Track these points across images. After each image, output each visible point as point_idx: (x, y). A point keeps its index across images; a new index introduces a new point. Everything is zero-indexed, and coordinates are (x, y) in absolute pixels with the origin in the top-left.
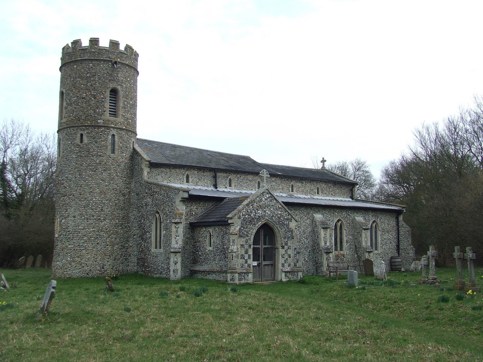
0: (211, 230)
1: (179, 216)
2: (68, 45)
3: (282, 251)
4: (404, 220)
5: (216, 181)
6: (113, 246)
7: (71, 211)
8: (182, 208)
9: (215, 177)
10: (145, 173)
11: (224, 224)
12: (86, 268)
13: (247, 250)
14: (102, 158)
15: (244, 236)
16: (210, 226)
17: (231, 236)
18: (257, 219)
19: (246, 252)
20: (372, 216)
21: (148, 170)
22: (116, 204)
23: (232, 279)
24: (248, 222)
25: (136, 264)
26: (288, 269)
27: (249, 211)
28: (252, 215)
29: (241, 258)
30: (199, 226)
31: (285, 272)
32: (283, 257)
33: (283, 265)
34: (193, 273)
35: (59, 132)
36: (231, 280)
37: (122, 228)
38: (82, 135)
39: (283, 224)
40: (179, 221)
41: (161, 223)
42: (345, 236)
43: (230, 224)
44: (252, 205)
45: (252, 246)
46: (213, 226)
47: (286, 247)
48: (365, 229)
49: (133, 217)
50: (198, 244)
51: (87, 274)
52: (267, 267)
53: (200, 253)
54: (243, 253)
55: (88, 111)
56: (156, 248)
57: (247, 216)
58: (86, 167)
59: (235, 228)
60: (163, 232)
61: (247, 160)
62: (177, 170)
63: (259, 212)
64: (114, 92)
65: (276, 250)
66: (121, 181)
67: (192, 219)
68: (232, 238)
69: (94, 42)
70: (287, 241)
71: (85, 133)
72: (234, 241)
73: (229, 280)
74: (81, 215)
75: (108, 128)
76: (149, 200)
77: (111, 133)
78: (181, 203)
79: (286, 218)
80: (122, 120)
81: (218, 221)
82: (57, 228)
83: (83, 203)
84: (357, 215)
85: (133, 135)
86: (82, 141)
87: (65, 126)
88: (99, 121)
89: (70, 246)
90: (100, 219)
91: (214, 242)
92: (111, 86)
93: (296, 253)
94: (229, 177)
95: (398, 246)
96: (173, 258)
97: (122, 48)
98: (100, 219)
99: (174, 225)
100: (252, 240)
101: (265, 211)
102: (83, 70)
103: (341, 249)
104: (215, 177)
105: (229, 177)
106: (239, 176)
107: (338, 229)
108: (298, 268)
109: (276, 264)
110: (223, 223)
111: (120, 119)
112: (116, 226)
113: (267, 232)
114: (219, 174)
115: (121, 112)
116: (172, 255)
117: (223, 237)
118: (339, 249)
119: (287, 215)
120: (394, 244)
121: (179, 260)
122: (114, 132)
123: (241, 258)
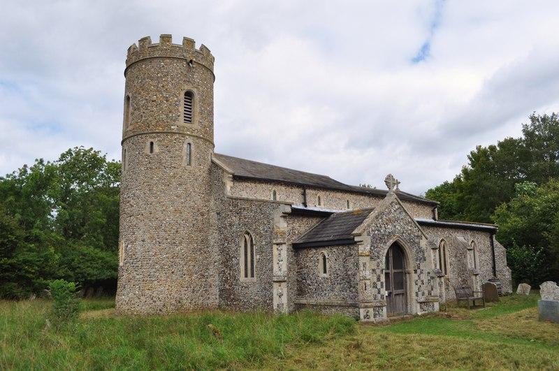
0: (325, 252)
1: (281, 235)
2: (134, 44)
3: (415, 277)
5: (305, 199)
6: (191, 275)
7: (139, 234)
8: (283, 225)
9: (304, 194)
10: (228, 188)
11: (347, 241)
12: (158, 303)
16: (324, 247)
17: (361, 258)
19: (379, 279)
20: (471, 235)
21: (231, 184)
22: (193, 225)
23: (367, 316)
24: (378, 239)
25: (218, 297)
26: (422, 299)
27: (378, 225)
29: (374, 287)
30: (305, 248)
31: (421, 303)
32: (417, 284)
33: (417, 295)
34: (299, 307)
35: (135, 71)
36: (365, 318)
37: (201, 253)
38: (152, 143)
39: (414, 243)
40: (282, 242)
41: (252, 245)
43: (356, 242)
44: (381, 218)
45: (384, 271)
46: (328, 246)
47: (419, 271)
48: (469, 250)
49: (214, 240)
50: (305, 271)
52: (398, 297)
53: (309, 282)
54: (375, 280)
56: (246, 276)
58: (158, 180)
59: (364, 248)
60: (257, 257)
61: (327, 179)
62: (264, 185)
64: (189, 95)
65: (408, 275)
67: (295, 239)
68: (362, 260)
69: (166, 38)
71: (155, 141)
72: (364, 265)
73: (362, 317)
75: (183, 135)
76: (235, 219)
77: (187, 141)
78: (282, 220)
81: (338, 240)
82: (122, 254)
83: (154, 224)
85: (211, 146)
86: (152, 151)
87: (132, 134)
88: (172, 127)
89: (138, 277)
91: (331, 267)
92: (187, 87)
94: (318, 195)
95: (494, 268)
96: (276, 289)
97: (197, 47)
99: (275, 247)
101: (395, 226)
104: (304, 194)
105: (318, 195)
106: (328, 193)
109: (408, 293)
110: (348, 242)
111: (196, 125)
112: (194, 251)
113: (397, 252)
114: (308, 191)
115: (197, 118)
116: (275, 285)
117: (345, 260)
120: (490, 266)
121: (285, 291)
122: (190, 140)
123: (374, 287)
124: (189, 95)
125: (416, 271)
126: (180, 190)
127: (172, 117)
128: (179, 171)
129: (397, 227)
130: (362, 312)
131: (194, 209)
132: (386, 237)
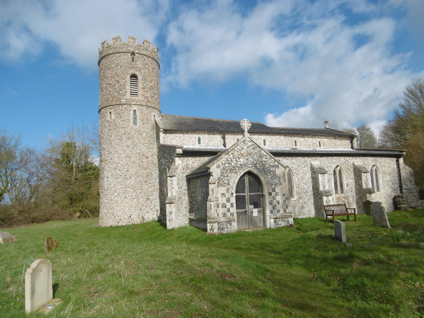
4: (405, 162)
9: (224, 138)
12: (117, 218)
13: (229, 198)
14: (126, 129)
15: (225, 185)
18: (239, 167)
19: (228, 200)
22: (139, 165)
23: (212, 229)
27: (229, 160)
28: (233, 164)
36: (210, 230)
38: (110, 113)
42: (345, 180)
47: (273, 194)
51: (118, 222)
54: (225, 202)
55: (113, 94)
57: (227, 165)
63: (240, 160)
66: (144, 146)
70: (274, 188)
72: (213, 190)
73: (208, 230)
74: (112, 175)
75: (130, 105)
77: (133, 109)
79: (271, 164)
80: (142, 99)
84: (356, 161)
88: (122, 100)
89: (106, 201)
90: (126, 178)
92: (132, 72)
93: (285, 199)
98: (126, 178)
100: (234, 189)
102: (109, 63)
103: (342, 192)
104: (224, 138)
107: (338, 174)
108: (288, 213)
118: (339, 192)
119: (273, 161)
122: (135, 108)
124: (134, 76)
125: (270, 194)
126: (129, 143)
127: (122, 93)
128: (128, 130)
129: (250, 159)
130: (209, 226)
131: (140, 154)
132: (237, 168)
